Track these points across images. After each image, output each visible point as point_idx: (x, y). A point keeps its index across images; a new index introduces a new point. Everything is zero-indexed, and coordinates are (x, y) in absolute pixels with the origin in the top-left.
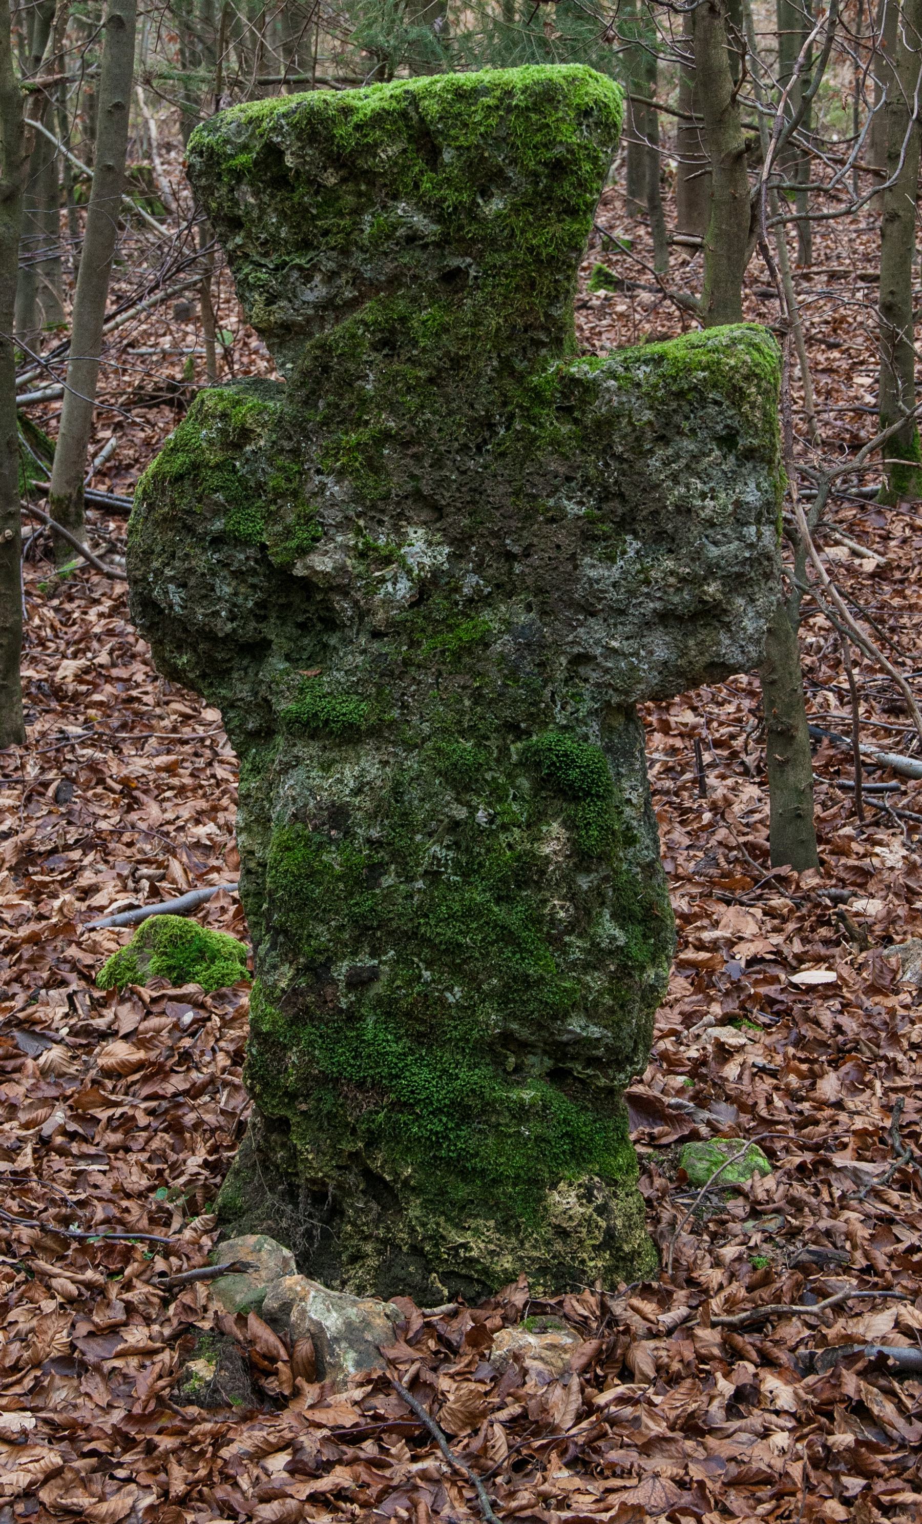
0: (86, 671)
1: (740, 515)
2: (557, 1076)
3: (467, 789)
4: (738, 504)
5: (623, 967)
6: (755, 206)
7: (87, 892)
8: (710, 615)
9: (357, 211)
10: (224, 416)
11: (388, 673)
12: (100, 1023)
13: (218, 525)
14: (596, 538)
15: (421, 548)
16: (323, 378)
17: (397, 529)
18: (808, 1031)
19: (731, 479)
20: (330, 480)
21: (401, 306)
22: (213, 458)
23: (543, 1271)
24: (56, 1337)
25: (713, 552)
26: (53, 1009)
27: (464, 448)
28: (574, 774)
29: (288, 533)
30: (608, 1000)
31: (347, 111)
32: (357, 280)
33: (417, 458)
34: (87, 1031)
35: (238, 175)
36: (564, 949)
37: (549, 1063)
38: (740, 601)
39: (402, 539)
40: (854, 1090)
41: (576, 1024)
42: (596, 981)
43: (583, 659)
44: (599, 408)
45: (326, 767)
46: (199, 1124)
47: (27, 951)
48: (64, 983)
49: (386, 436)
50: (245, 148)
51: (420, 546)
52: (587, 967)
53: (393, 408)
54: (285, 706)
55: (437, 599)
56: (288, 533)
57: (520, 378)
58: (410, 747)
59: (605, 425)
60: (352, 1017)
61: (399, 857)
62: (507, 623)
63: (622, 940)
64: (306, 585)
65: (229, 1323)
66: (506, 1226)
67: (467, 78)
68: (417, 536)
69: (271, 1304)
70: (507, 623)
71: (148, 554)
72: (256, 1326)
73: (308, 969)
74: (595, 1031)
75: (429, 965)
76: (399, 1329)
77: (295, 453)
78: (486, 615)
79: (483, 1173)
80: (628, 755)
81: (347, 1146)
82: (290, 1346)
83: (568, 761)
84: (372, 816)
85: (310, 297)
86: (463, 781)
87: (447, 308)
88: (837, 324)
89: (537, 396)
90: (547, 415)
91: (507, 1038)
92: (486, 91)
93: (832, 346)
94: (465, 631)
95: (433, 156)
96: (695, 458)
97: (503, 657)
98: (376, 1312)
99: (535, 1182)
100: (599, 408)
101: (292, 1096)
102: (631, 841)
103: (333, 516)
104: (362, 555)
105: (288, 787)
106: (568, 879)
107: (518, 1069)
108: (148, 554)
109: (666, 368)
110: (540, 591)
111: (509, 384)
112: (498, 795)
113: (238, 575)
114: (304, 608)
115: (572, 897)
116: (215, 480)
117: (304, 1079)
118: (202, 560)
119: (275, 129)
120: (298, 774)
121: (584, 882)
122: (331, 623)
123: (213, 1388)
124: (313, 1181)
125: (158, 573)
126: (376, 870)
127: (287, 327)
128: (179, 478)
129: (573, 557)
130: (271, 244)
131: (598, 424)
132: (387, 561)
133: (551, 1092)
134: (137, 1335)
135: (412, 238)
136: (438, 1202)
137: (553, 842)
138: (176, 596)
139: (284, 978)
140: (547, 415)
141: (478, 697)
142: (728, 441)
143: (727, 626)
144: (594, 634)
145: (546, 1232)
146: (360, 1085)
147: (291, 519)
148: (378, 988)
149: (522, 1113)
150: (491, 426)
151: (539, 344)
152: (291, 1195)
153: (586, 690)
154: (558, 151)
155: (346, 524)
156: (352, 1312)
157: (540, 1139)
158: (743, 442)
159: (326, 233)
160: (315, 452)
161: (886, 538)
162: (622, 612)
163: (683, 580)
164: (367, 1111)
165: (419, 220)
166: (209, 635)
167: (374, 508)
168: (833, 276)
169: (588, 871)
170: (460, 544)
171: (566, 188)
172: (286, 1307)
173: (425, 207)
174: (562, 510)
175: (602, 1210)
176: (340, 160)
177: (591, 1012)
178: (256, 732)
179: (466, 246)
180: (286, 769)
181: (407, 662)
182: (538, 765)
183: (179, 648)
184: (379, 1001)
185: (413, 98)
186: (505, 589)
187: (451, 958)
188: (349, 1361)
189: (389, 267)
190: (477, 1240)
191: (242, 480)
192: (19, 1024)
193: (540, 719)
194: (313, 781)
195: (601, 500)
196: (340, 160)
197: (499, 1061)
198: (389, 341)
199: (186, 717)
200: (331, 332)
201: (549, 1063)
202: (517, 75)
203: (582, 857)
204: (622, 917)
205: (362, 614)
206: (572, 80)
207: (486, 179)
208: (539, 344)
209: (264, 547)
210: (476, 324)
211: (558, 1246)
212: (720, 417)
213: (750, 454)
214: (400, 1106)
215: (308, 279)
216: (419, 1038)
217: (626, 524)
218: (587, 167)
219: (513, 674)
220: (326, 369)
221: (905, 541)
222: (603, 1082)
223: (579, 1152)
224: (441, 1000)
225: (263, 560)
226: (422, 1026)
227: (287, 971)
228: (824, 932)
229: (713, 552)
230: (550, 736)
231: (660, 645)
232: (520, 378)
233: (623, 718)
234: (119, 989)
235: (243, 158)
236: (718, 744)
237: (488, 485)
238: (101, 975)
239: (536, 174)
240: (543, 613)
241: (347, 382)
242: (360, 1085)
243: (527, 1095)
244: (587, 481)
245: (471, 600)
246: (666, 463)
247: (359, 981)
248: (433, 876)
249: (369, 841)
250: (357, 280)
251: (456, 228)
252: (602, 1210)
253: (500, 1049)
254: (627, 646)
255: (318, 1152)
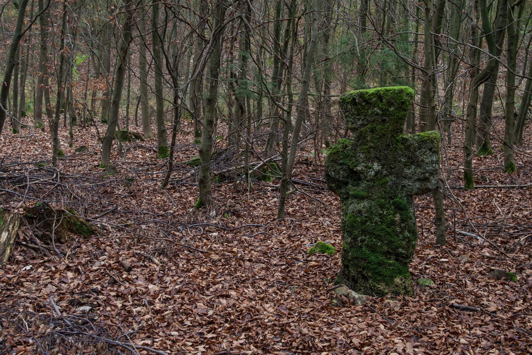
0: (294, 210)
1: (432, 162)
2: (397, 260)
3: (383, 208)
4: (432, 160)
5: (409, 240)
6: (437, 117)
7: (302, 242)
8: (426, 179)
9: (368, 109)
10: (343, 143)
11: (370, 187)
12: (309, 259)
13: (341, 161)
14: (407, 165)
15: (376, 166)
16: (361, 137)
17: (372, 163)
18: (442, 267)
19: (431, 156)
20: (361, 154)
21: (375, 125)
22: (341, 150)
23: (393, 292)
24: (309, 296)
25: (427, 168)
26: (300, 257)
27: (385, 149)
28: (401, 206)
29: (353, 163)
30: (406, 246)
31: (367, 93)
32: (367, 120)
33: (376, 151)
34: (306, 260)
35: (348, 103)
36: (399, 237)
37: (395, 257)
38: (432, 177)
39: (373, 165)
40: (450, 275)
41: (400, 250)
42: (404, 243)
43: (404, 186)
44: (408, 143)
45: (358, 204)
46: (329, 274)
47: (294, 248)
48: (301, 253)
49: (371, 147)
50: (349, 99)
51: (376, 166)
52: (403, 240)
53: (373, 142)
54: (351, 193)
55: (379, 175)
56: (353, 163)
57: (395, 138)
58: (373, 200)
59: (409, 146)
60: (361, 247)
61: (370, 219)
62: (391, 179)
63: (409, 236)
64: (356, 172)
65: (339, 296)
66: (386, 285)
67: (388, 88)
68: (376, 164)
69: (346, 294)
70: (391, 179)
71: (328, 166)
72: (343, 297)
73: (353, 238)
74: (404, 252)
75: (375, 238)
76: (368, 299)
77: (355, 150)
78: (387, 178)
79: (383, 275)
80: (411, 204)
81: (359, 270)
82: (349, 300)
83: (401, 203)
84: (366, 212)
85: (359, 123)
86: (382, 206)
87: (383, 126)
88: (456, 156)
89: (398, 141)
90: (399, 144)
91: (388, 252)
92: (391, 90)
93: (454, 160)
94: (384, 181)
95: (381, 101)
96: (425, 152)
97: (390, 185)
98: (364, 297)
99: (392, 277)
100: (408, 143)
101: (350, 261)
102: (411, 219)
103: (361, 160)
104: (366, 167)
105: (351, 207)
106: (400, 224)
107: (390, 258)
108: (328, 166)
109: (420, 137)
110: (397, 174)
111: (393, 139)
112: (388, 209)
113: (344, 170)
114: (355, 176)
115: (400, 227)
116: (341, 154)
117: (352, 258)
118: (338, 167)
119: (355, 95)
120: (353, 205)
121: (403, 225)
122: (360, 179)
123: (337, 304)
124: (352, 276)
125: (330, 170)
126: (366, 221)
127: (355, 128)
128: (334, 153)
129: (403, 169)
130: (353, 114)
131: (408, 146)
132: (370, 168)
133: (396, 262)
134: (323, 297)
135: (377, 114)
136: (375, 280)
137: (397, 218)
138: (333, 173)
139: (349, 240)
140: (399, 144)
141: (385, 192)
142: (430, 149)
143: (429, 182)
144: (406, 182)
145: (394, 286)
146: (362, 259)
147: (354, 161)
148: (366, 242)
149: (390, 265)
150: (390, 146)
151: (398, 132)
152: (348, 279)
153: (404, 192)
154: (403, 100)
155: (363, 162)
156: (360, 295)
157: (393, 269)
158: (433, 150)
159: (362, 113)
160: (358, 149)
161: (464, 197)
162: (411, 178)
163: (422, 173)
164: (363, 263)
165: (378, 111)
166: (338, 180)
167: (368, 159)
168: (456, 147)
169: (403, 223)
170: (383, 165)
171: (404, 106)
172: (348, 294)
173: (380, 109)
174: (401, 160)
175: (404, 282)
176: (365, 101)
177: (403, 248)
178: (345, 198)
179: (386, 115)
180: (351, 204)
181: (373, 186)
182: (395, 204)
183: (333, 183)
184: (366, 244)
185: (378, 91)
186: (391, 174)
187: (379, 237)
188: (359, 302)
189: (373, 119)
190: (382, 287)
191: (346, 154)
192: (294, 259)
193: (396, 196)
194: (355, 206)
195: (408, 159)
196: (365, 101)
197: (386, 256)
198: (372, 131)
199: (316, 219)
200: (362, 129)
201: (395, 257)
202: (396, 88)
203: (403, 220)
204: (409, 231)
205: (365, 177)
206: (406, 89)
207: (390, 104)
208: (398, 132)
209: (349, 166)
210: (388, 128)
211: (396, 288)
212: (430, 145)
213: (434, 152)
214: (369, 263)
215: (359, 120)
216: (372, 251)
217: (412, 163)
218: (408, 103)
219: (392, 188)
220: (361, 135)
221: (469, 197)
222: (405, 261)
223: (400, 273)
224: (377, 245)
225: (349, 168)
226: (373, 249)
227: (350, 239)
228: (446, 255)
229: (427, 168)
230: (398, 199)
231: (418, 185)
232: (395, 138)
233: (410, 197)
234: (312, 253)
235: (349, 100)
236: (426, 229)
237: (388, 156)
238: (308, 252)
239: (399, 104)
240: (397, 178)
241: (365, 138)
242: (362, 259)
243: (391, 262)
244: (406, 155)
245: (384, 176)
246: (420, 153)
247: (362, 241)
248: (376, 223)
249: (365, 216)
250: (367, 120)
251: (385, 112)
252: (404, 282)
253: (387, 254)
254: (412, 184)
255: (354, 271)
